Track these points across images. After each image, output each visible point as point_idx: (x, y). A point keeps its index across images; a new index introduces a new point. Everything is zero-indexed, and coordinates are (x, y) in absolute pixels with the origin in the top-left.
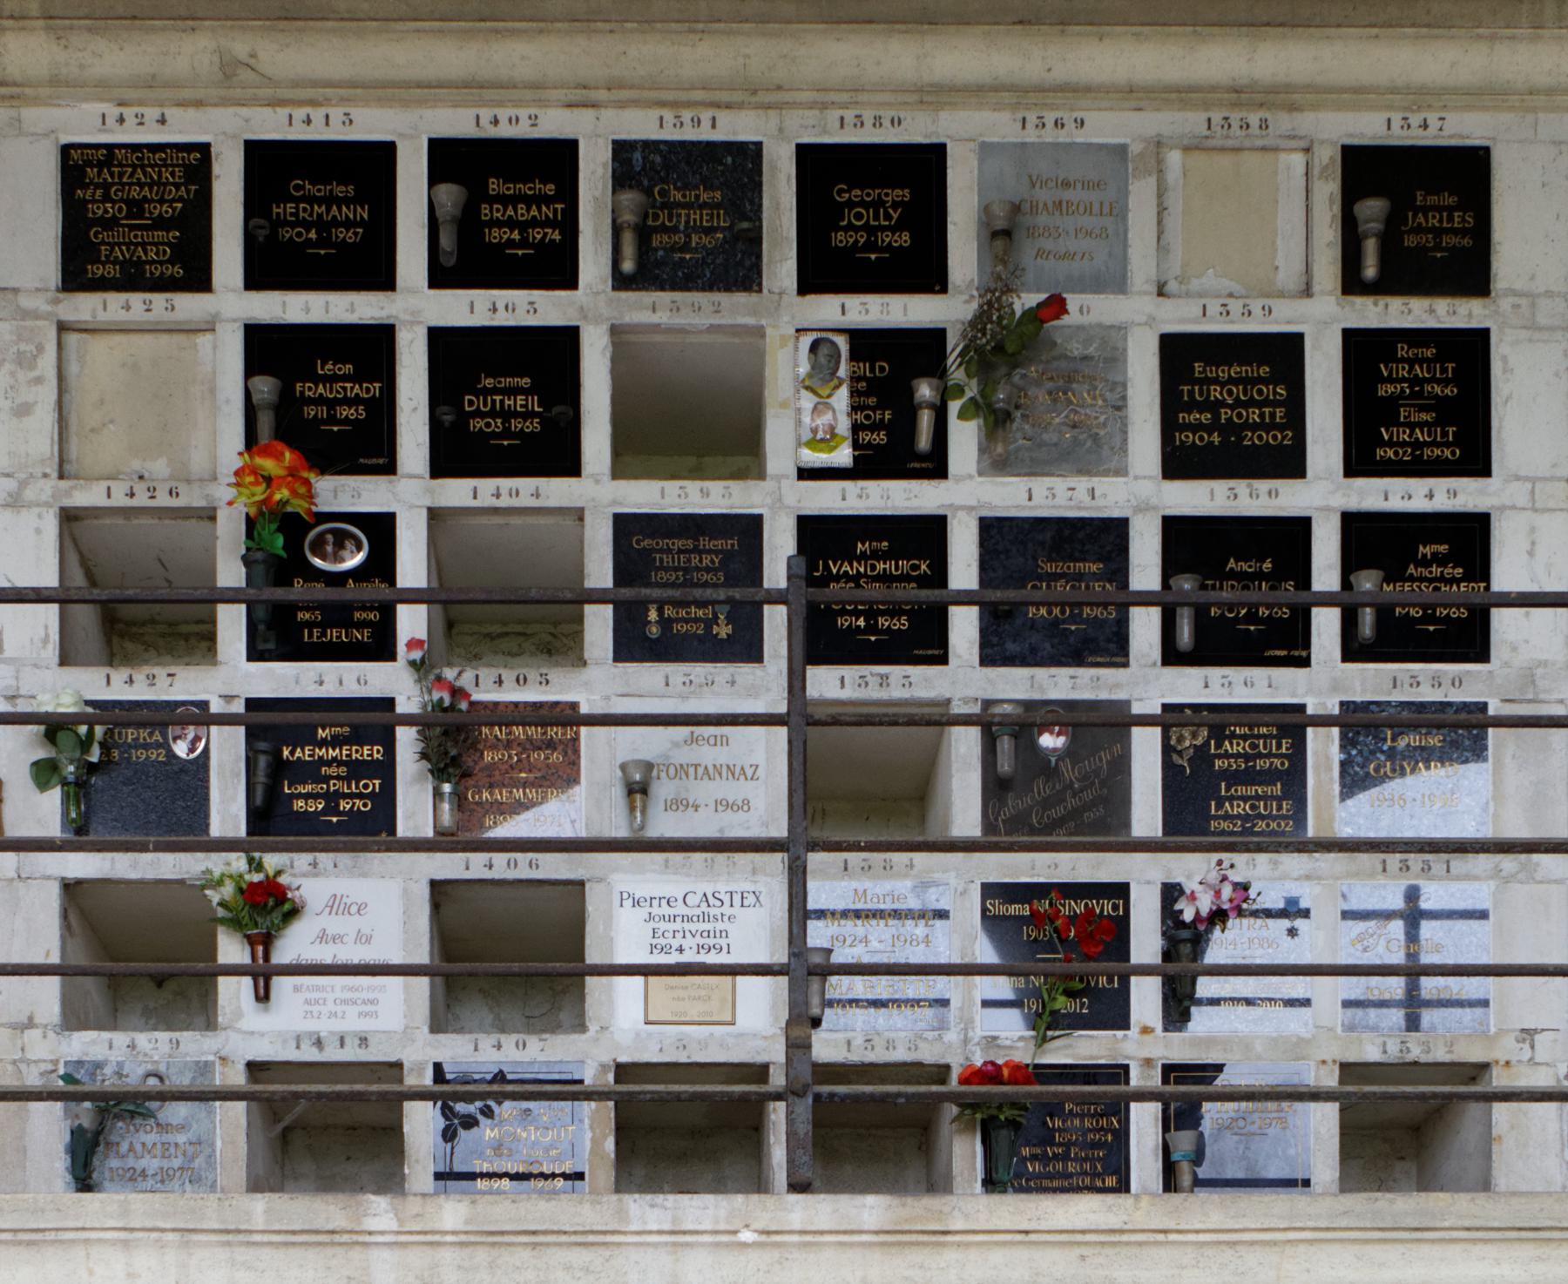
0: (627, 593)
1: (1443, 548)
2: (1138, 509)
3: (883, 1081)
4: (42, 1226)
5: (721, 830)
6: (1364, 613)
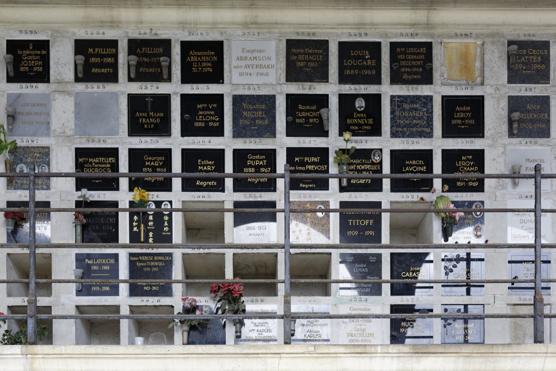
2: (174, 93)
5: (278, 189)
6: (343, 181)
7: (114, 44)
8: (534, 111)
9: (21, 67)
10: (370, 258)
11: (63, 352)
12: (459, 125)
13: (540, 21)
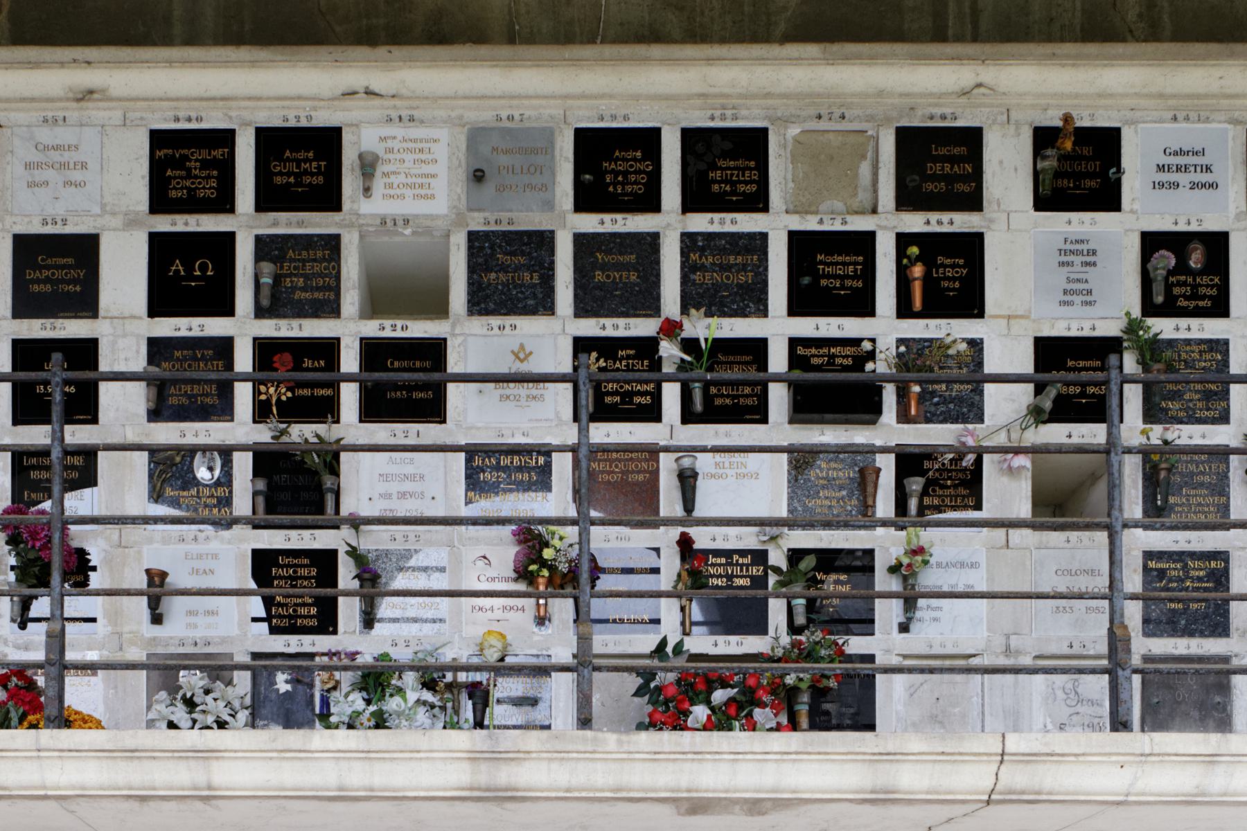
0: (22, 375)
1: (632, 352)
3: (197, 660)
4: (829, 751)
8: (68, 282)
9: (172, 189)
10: (711, 560)
11: (436, 748)
12: (835, 289)
13: (6, 86)
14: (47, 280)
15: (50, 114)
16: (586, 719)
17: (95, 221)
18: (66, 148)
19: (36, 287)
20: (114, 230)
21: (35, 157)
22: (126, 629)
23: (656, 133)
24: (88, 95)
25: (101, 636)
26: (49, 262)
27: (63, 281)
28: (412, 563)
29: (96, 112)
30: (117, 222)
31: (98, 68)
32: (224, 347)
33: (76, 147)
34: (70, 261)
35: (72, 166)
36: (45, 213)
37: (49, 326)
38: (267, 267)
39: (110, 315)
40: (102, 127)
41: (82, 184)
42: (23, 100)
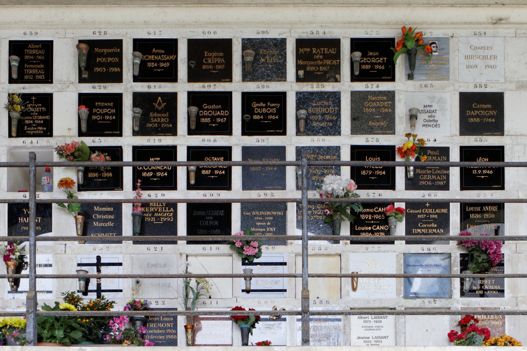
7: (335, 43)
14: (477, 116)
15: (477, 31)
16: (306, 340)
17: (502, 86)
18: (486, 48)
19: (472, 119)
20: (512, 90)
21: (470, 52)
22: (519, 295)
23: (176, 41)
24: (499, 21)
25: (507, 299)
26: (478, 106)
27: (485, 117)
28: (256, 260)
29: (502, 30)
30: (513, 86)
31: (508, 7)
32: (281, 151)
33: (491, 48)
34: (489, 106)
35: (489, 57)
36: (475, 82)
37: (478, 140)
38: (194, 109)
39: (510, 134)
40: (505, 37)
41: (495, 67)
42: (466, 23)
